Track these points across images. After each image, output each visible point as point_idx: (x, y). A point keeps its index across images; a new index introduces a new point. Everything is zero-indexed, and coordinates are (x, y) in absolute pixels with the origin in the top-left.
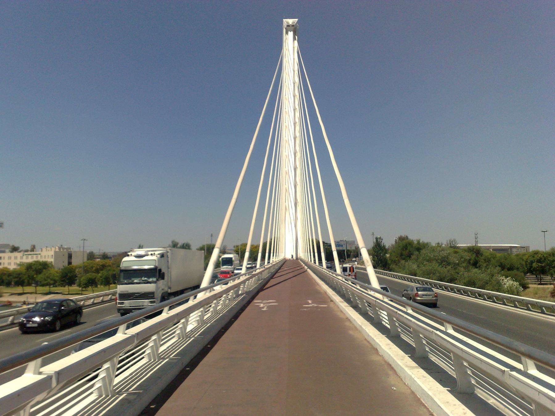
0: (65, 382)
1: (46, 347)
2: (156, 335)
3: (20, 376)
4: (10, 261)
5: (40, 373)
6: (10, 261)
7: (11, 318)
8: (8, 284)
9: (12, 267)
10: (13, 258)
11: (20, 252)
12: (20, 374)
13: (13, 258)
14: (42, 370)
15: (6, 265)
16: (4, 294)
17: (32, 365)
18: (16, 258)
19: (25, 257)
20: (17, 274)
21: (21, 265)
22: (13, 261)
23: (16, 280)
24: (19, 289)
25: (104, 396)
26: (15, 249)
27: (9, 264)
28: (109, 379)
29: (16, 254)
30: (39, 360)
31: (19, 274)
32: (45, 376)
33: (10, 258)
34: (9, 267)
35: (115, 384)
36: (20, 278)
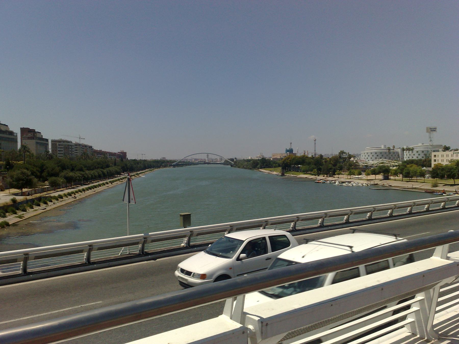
0: (285, 334)
1: (452, 235)
2: (423, 293)
3: (217, 316)
4: (442, 158)
5: (448, 258)
6: (442, 158)
7: (409, 209)
8: (442, 177)
9: (445, 163)
10: (445, 156)
11: (451, 151)
12: (429, 255)
13: (445, 156)
14: (449, 255)
15: (440, 162)
16: (439, 185)
17: (439, 249)
18: (447, 156)
19: (455, 155)
20: (448, 169)
21: (451, 161)
22: (445, 158)
23: (448, 173)
24: (451, 181)
25: (418, 336)
26: (446, 149)
27: (442, 160)
28: (424, 315)
29: (447, 152)
30: (447, 246)
31: (451, 169)
32: (453, 262)
33: (442, 156)
34: (442, 163)
35: (435, 322)
36: (452, 172)
